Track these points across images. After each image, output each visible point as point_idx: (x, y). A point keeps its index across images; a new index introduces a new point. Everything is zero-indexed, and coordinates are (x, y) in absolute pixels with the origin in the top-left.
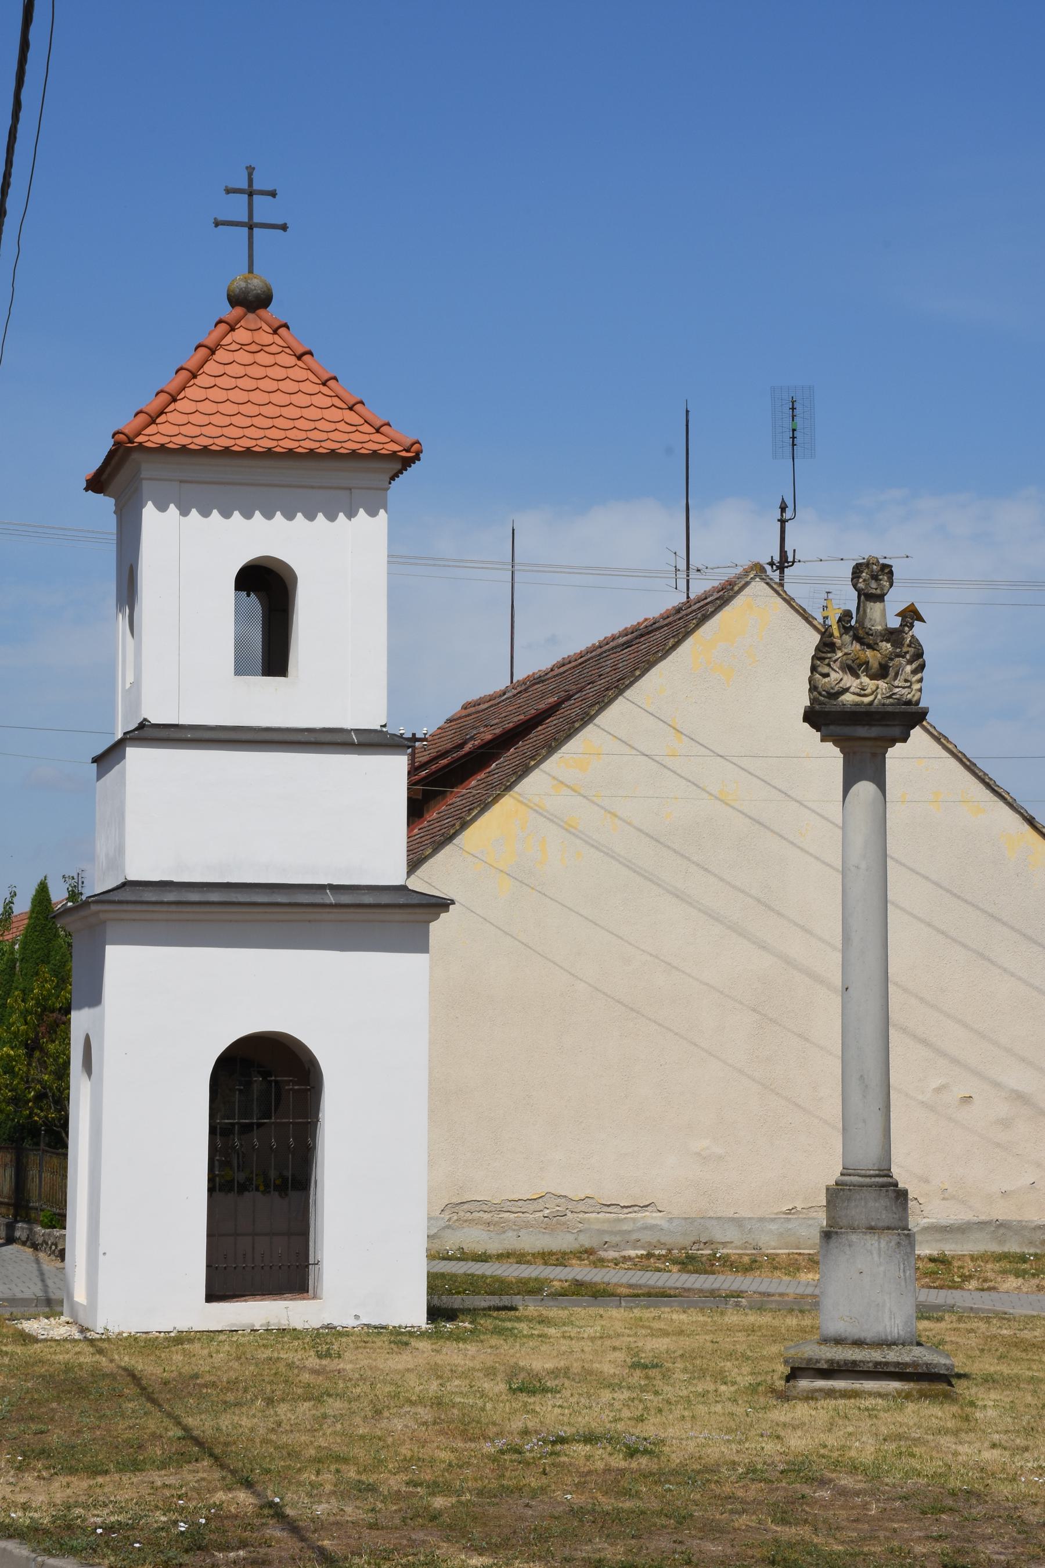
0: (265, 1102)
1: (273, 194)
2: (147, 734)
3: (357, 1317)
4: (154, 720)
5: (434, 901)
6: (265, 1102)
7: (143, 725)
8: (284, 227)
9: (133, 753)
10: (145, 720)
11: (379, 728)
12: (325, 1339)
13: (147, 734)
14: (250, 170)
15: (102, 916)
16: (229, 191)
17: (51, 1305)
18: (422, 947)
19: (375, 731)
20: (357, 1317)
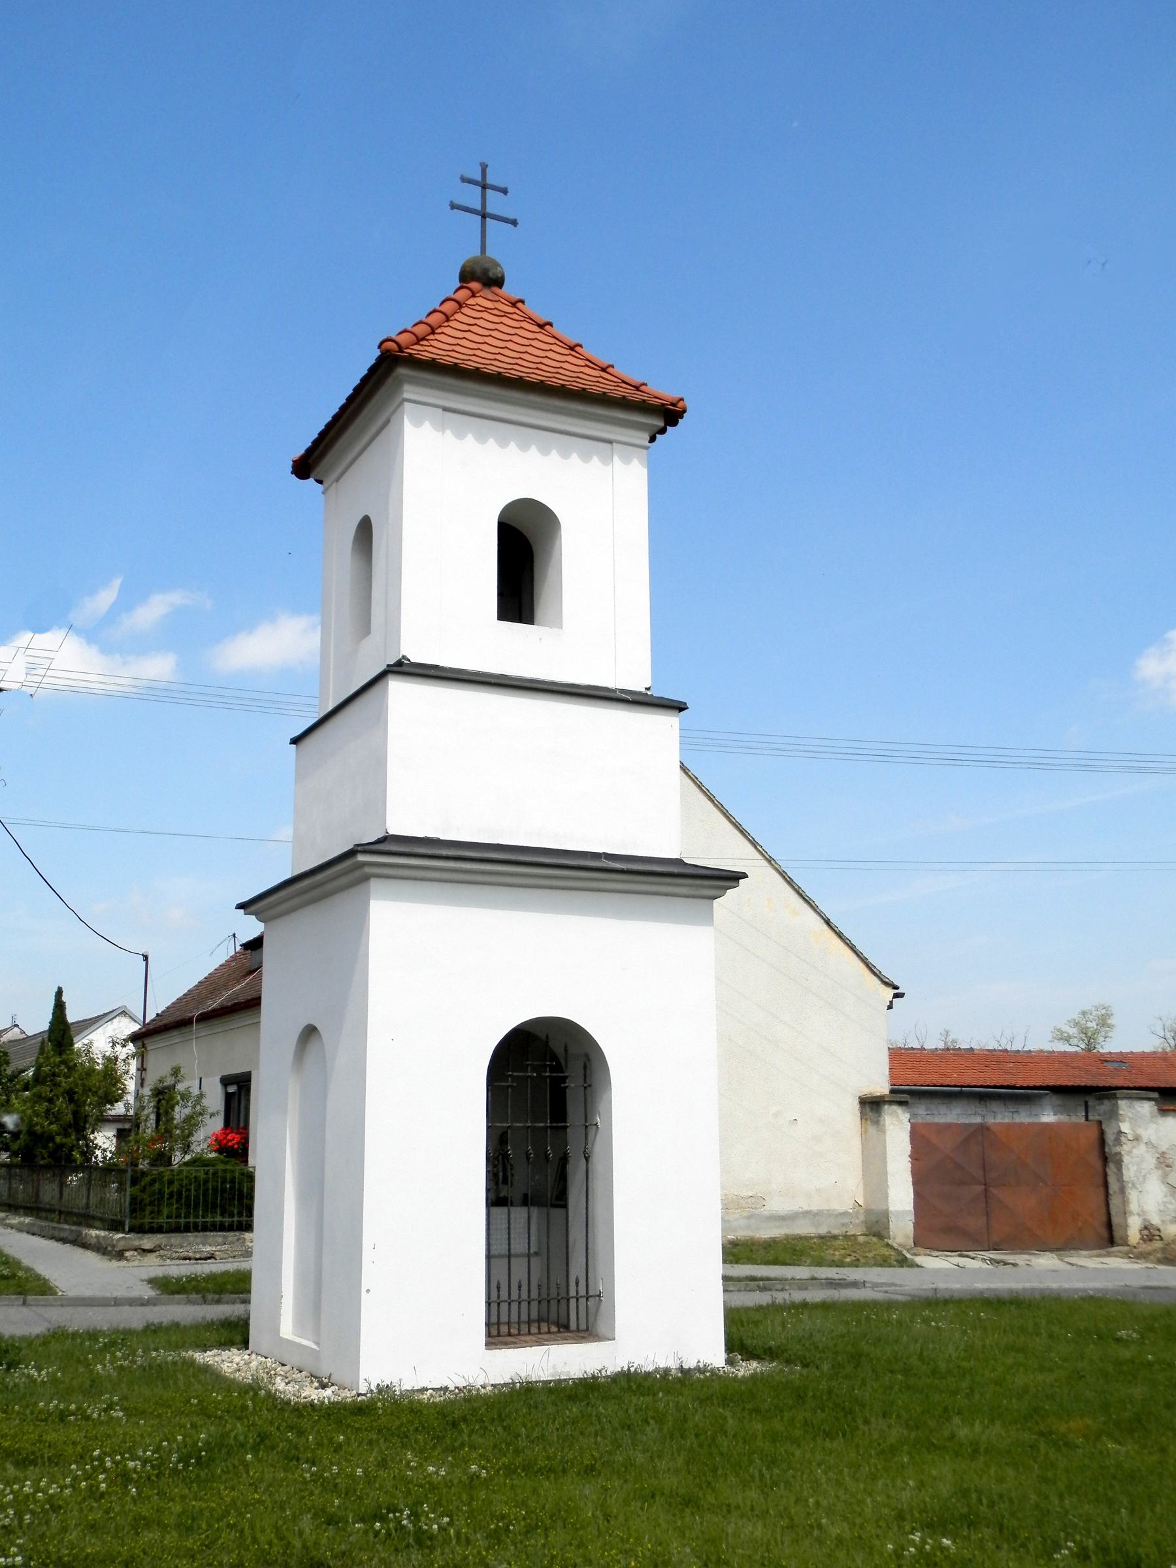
0: (543, 1091)
1: (505, 191)
2: (402, 668)
3: (368, 1291)
4: (414, 659)
5: (717, 873)
6: (543, 1091)
7: (399, 663)
8: (514, 223)
9: (396, 687)
10: (404, 657)
11: (643, 690)
12: (631, 1384)
13: (402, 668)
14: (484, 168)
15: (367, 870)
16: (464, 180)
17: (236, 1333)
18: (708, 919)
19: (640, 693)
20: (368, 1291)
